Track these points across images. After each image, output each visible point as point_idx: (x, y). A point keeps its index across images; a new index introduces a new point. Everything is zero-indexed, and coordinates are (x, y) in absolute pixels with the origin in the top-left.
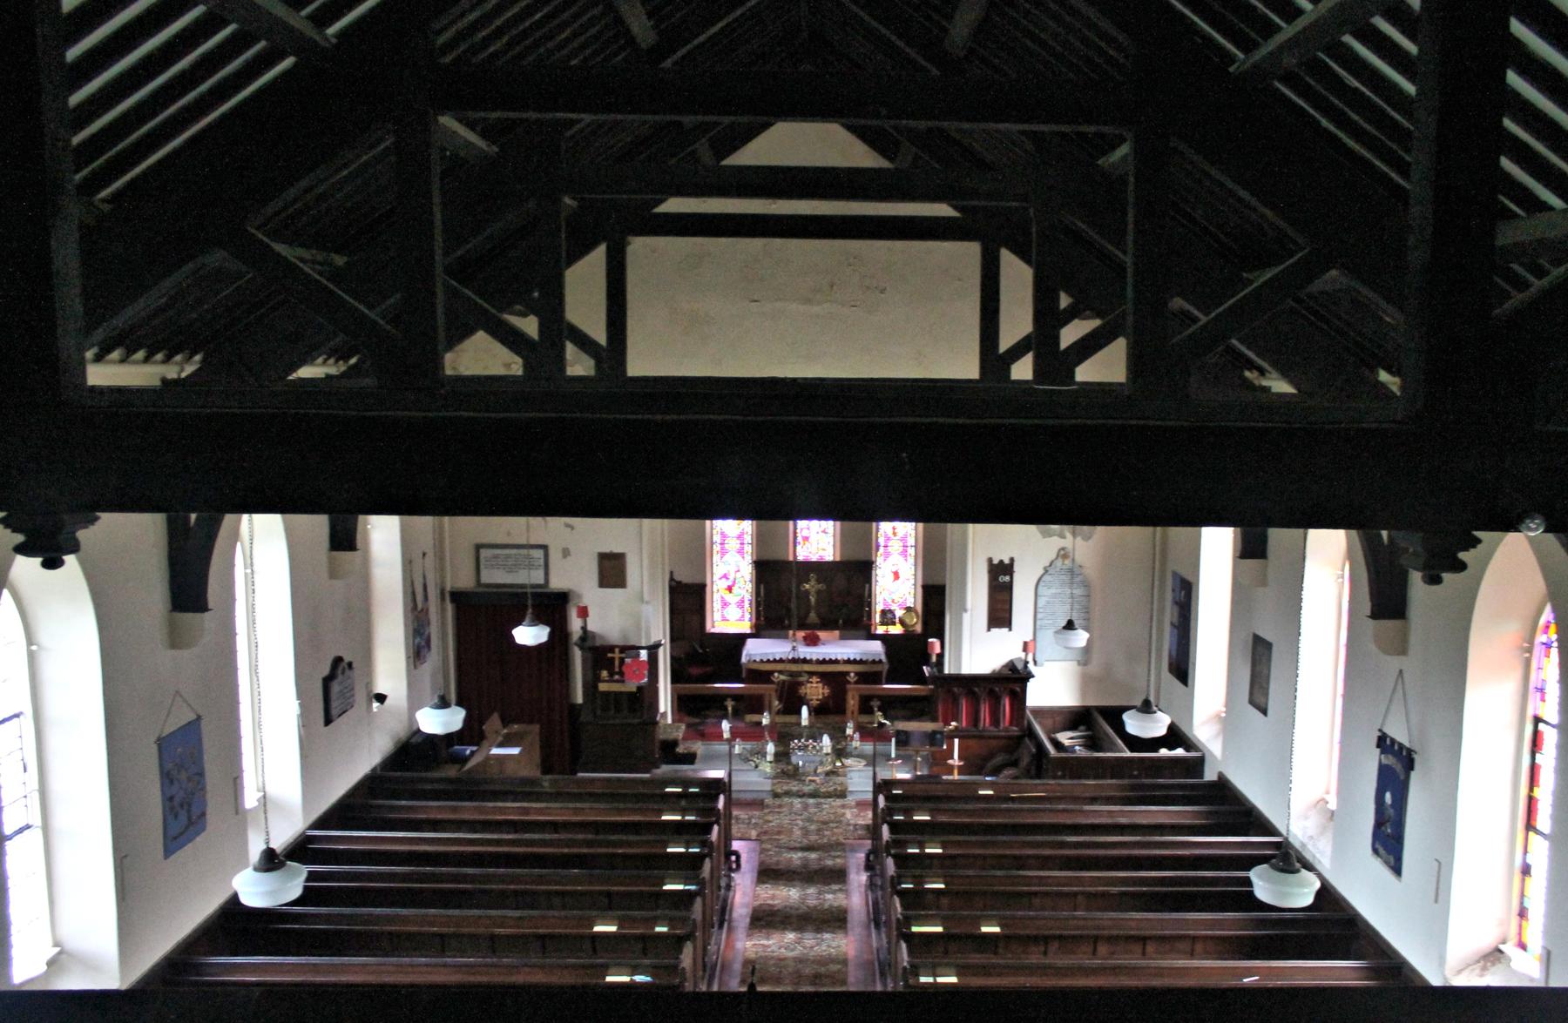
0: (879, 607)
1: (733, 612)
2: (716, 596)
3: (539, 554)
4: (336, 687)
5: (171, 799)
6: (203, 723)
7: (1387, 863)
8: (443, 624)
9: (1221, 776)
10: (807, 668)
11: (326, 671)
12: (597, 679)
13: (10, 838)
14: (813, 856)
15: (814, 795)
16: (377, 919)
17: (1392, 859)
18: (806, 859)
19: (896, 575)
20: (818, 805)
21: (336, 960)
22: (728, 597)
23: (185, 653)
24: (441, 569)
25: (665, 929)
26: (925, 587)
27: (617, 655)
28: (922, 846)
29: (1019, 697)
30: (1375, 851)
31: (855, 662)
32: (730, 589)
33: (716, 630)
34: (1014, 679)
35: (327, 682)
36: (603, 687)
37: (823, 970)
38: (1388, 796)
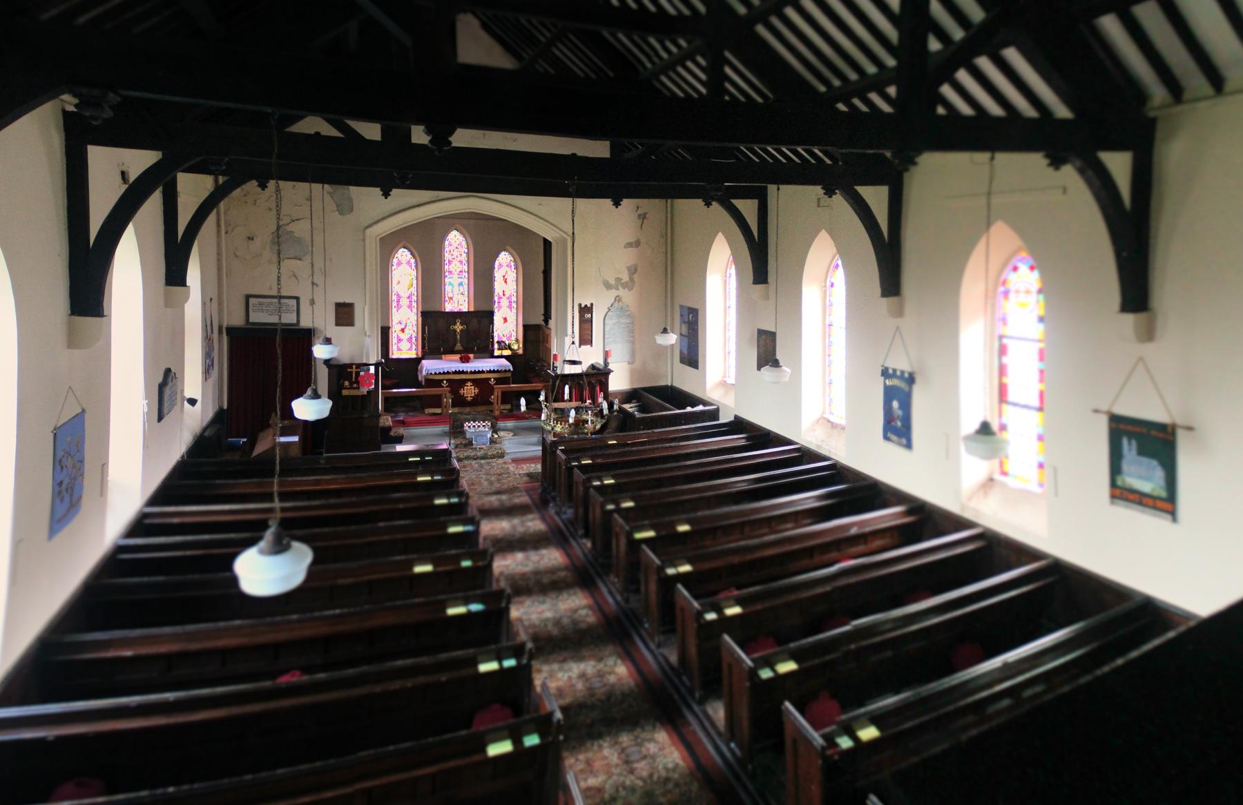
0: (496, 339)
1: (405, 345)
2: (395, 335)
3: (294, 302)
4: (167, 391)
5: (61, 484)
6: (87, 417)
7: (900, 444)
8: (220, 349)
9: (736, 417)
10: (464, 377)
11: (160, 379)
12: (342, 387)
13: (606, 364)
14: (504, 497)
15: (483, 458)
16: (725, 485)
17: (904, 441)
18: (500, 500)
19: (505, 320)
20: (488, 464)
21: (210, 625)
22: (402, 336)
23: (76, 351)
24: (220, 312)
25: (428, 568)
26: (526, 327)
27: (354, 370)
28: (600, 479)
29: (604, 386)
30: (886, 438)
31: (494, 371)
32: (403, 330)
33: (394, 357)
34: (598, 376)
35: (162, 387)
36: (345, 392)
37: (555, 577)
38: (895, 404)
